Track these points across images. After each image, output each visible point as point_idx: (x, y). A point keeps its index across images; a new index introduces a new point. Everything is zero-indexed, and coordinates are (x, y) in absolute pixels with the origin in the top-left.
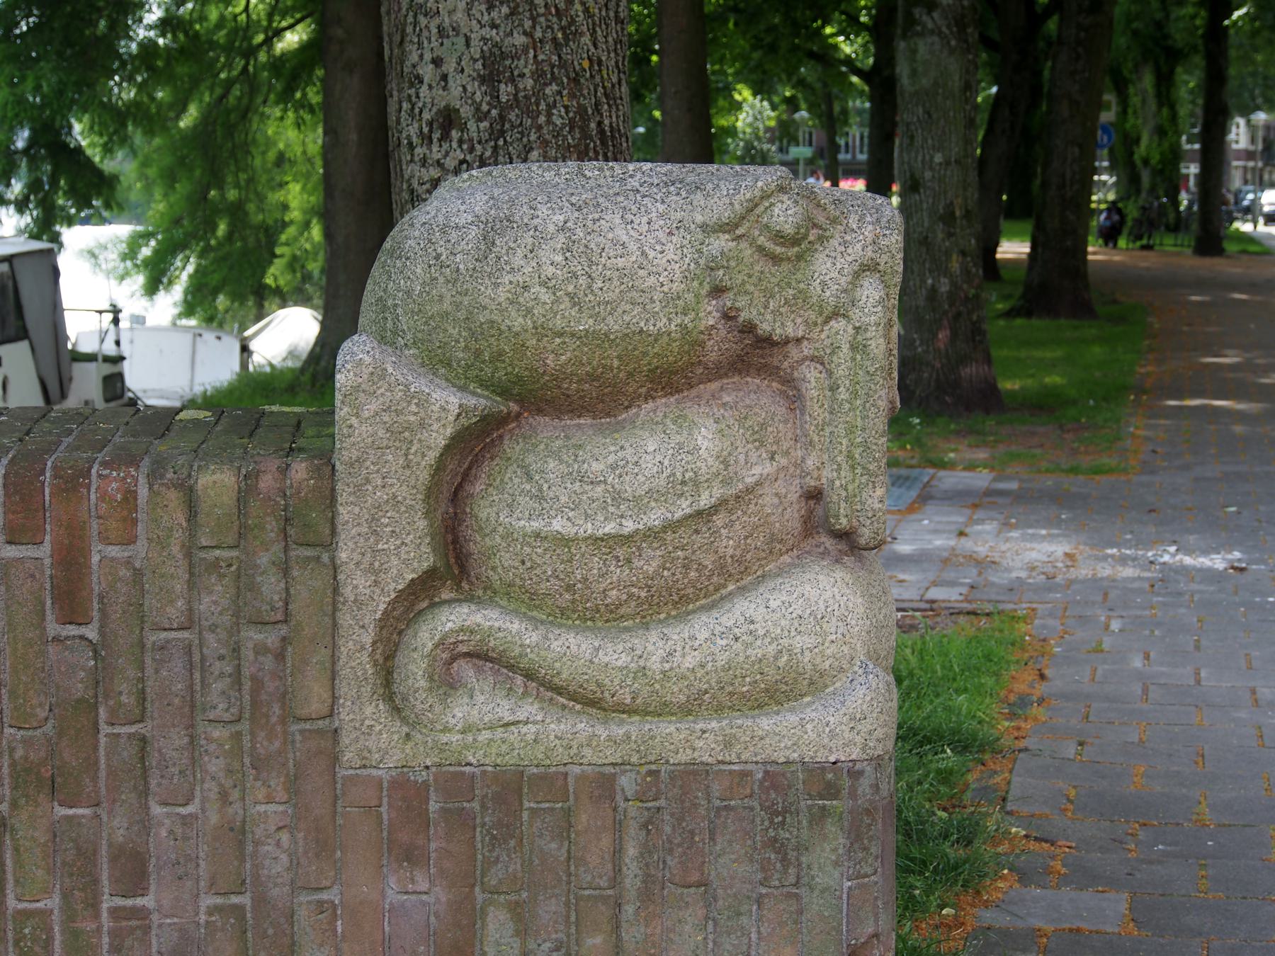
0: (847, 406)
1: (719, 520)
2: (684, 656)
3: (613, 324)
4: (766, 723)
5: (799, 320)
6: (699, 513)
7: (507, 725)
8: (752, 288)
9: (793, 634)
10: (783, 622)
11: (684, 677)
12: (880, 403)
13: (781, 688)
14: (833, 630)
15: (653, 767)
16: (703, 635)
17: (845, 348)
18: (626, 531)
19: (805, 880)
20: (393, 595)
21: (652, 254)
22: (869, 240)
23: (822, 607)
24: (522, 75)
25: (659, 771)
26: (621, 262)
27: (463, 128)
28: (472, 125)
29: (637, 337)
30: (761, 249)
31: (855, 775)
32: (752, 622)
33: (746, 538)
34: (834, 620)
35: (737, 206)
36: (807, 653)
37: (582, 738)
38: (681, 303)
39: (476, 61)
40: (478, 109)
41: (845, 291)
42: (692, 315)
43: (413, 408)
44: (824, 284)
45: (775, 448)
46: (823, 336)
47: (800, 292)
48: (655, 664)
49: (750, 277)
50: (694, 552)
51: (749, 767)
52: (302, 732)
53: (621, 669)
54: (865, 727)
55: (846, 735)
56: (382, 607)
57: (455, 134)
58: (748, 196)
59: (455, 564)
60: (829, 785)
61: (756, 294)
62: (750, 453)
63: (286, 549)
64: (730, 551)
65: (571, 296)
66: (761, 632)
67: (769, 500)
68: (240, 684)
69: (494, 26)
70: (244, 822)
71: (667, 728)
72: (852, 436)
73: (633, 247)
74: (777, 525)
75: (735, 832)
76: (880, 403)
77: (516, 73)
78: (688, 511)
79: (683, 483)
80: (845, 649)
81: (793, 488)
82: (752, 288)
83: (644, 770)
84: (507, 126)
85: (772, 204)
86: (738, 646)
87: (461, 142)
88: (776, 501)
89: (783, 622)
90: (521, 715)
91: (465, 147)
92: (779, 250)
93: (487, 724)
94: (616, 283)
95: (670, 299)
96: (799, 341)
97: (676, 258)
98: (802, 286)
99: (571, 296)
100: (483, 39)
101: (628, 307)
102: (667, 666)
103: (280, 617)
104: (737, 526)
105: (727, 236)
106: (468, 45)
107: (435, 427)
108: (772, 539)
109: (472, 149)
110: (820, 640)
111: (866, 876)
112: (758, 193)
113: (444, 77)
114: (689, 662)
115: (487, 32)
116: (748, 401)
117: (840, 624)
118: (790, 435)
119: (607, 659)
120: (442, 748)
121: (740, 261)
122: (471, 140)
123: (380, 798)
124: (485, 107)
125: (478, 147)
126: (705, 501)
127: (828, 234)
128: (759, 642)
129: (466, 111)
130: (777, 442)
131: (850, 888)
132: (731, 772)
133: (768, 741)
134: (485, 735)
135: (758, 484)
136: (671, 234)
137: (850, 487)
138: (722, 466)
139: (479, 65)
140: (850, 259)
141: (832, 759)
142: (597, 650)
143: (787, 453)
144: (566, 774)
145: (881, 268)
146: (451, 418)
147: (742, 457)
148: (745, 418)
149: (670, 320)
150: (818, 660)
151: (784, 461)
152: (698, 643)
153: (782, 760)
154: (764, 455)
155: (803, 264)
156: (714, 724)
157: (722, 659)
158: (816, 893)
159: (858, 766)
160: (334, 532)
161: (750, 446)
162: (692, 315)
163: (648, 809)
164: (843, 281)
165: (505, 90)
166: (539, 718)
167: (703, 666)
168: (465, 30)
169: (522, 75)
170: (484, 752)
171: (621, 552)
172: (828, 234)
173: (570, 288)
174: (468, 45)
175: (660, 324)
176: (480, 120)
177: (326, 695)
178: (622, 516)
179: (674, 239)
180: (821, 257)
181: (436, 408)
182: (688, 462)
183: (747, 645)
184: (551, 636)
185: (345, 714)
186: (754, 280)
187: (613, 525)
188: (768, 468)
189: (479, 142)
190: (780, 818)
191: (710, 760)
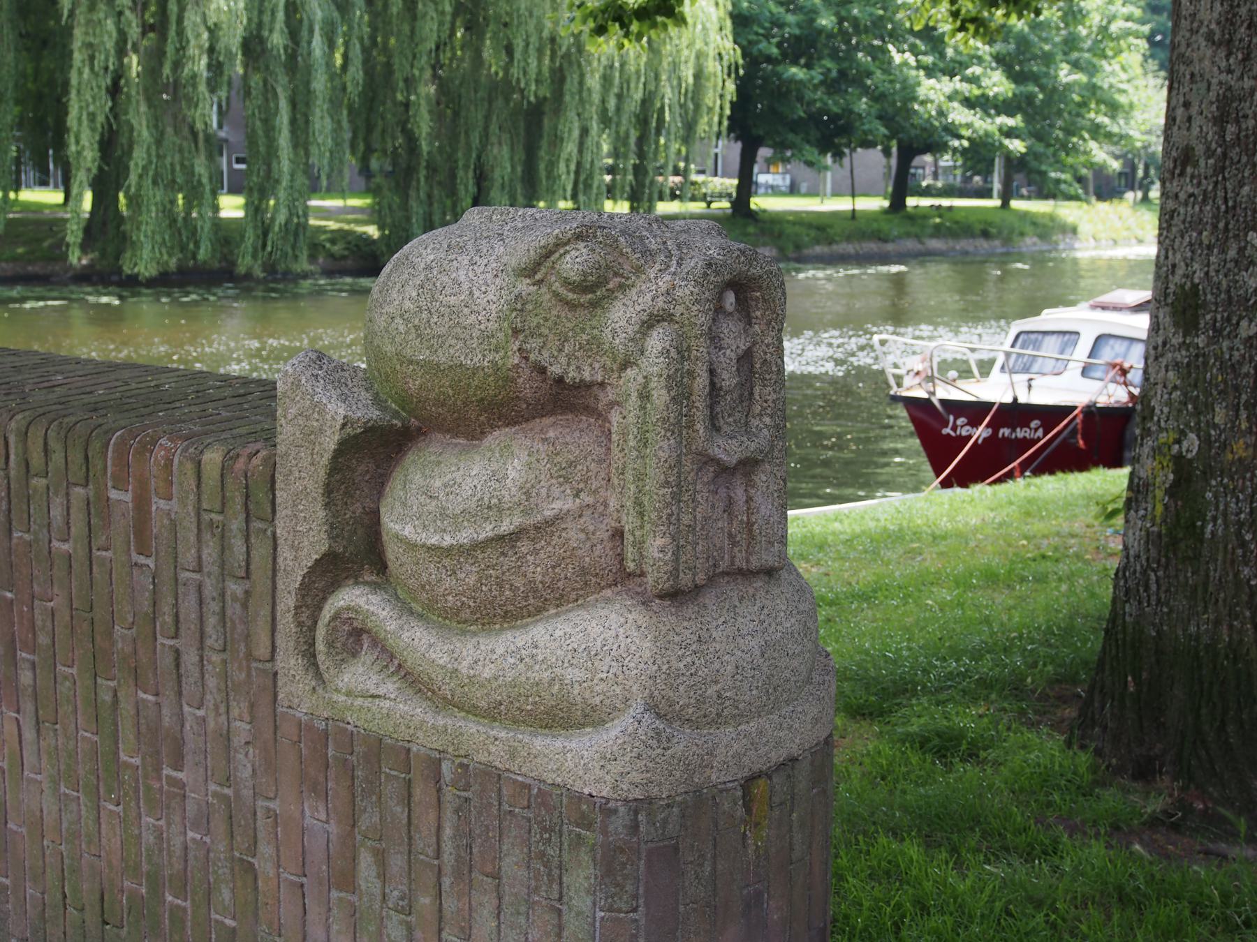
0: (635, 453)
1: (524, 546)
2: (484, 666)
3: (442, 357)
4: (540, 743)
5: (597, 365)
6: (500, 538)
7: (373, 696)
8: (546, 332)
9: (566, 665)
10: (559, 652)
11: (483, 686)
12: (661, 453)
13: (560, 716)
14: (605, 668)
15: (465, 761)
16: (500, 651)
17: (634, 395)
18: (445, 544)
19: (565, 899)
20: (306, 570)
21: (477, 293)
22: (663, 290)
23: (599, 644)
24: (1246, 117)
25: (468, 766)
26: (452, 300)
27: (1196, 165)
28: (1202, 163)
29: (459, 370)
30: (556, 294)
31: (608, 812)
32: (536, 647)
33: (554, 567)
34: (608, 659)
35: (532, 252)
36: (576, 686)
37: (417, 720)
38: (493, 341)
39: (1212, 103)
40: (1208, 148)
41: (633, 340)
42: (502, 354)
43: (316, 415)
44: (614, 331)
45: (582, 485)
46: (621, 383)
47: (593, 338)
48: (464, 667)
49: (546, 320)
50: (503, 573)
51: (528, 781)
52: (257, 668)
53: (443, 667)
54: (616, 768)
55: (597, 771)
56: (300, 578)
57: (1189, 170)
58: (542, 243)
59: (359, 552)
60: (583, 816)
61: (551, 337)
62: (553, 488)
63: (247, 520)
64: (540, 578)
65: (417, 328)
66: (540, 658)
67: (573, 534)
68: (225, 623)
69: (1230, 71)
70: (228, 731)
71: (472, 728)
72: (640, 484)
73: (465, 286)
74: (587, 559)
75: (516, 837)
76: (661, 453)
77: (1241, 114)
78: (490, 534)
79: (489, 508)
80: (618, 690)
81: (603, 526)
82: (546, 332)
83: (458, 761)
84: (1227, 163)
85: (567, 252)
86: (521, 666)
87: (1192, 177)
88: (582, 536)
89: (559, 652)
90: (381, 691)
91: (1195, 181)
92: (571, 296)
93: (362, 693)
94: (447, 319)
95: (486, 336)
96: (602, 385)
97: (495, 299)
98: (596, 332)
99: (417, 328)
100: (1220, 83)
101: (453, 342)
102: (472, 672)
103: (243, 574)
104: (542, 555)
105: (528, 281)
106: (1209, 89)
107: (328, 433)
108: (583, 571)
109: (1199, 184)
110: (589, 676)
111: (620, 911)
112: (552, 240)
113: (1189, 119)
114: (487, 673)
115: (1223, 77)
116: (568, 439)
117: (614, 664)
118: (602, 474)
119: (434, 656)
120: (332, 704)
121: (538, 304)
122: (1199, 175)
123: (300, 736)
124: (1214, 146)
125: (1204, 181)
126: (506, 527)
127: (629, 282)
128: (537, 667)
129: (1200, 149)
130: (586, 481)
131: (602, 918)
132: (515, 781)
133: (539, 760)
134: (359, 701)
135: (558, 518)
136: (496, 276)
137: (637, 533)
138: (524, 497)
139: (1214, 108)
140: (638, 308)
141: (586, 791)
142: (431, 646)
143: (595, 492)
144: (409, 750)
145: (677, 319)
146: (338, 427)
147: (544, 492)
148: (557, 454)
149: (484, 356)
150: (587, 695)
151: (589, 500)
152: (494, 657)
153: (550, 781)
154: (568, 491)
155: (599, 311)
156: (503, 734)
157: (510, 675)
158: (573, 914)
159: (611, 805)
160: (274, 512)
161: (554, 481)
162: (502, 354)
163: (459, 797)
164: (630, 329)
165: (1231, 129)
166: (393, 696)
167: (496, 679)
168: (1207, 76)
169: (1246, 117)
170: (361, 716)
171: (446, 562)
172: (629, 282)
173: (416, 322)
174: (1209, 89)
175: (475, 360)
176: (1209, 158)
177: (268, 643)
178: (445, 531)
179: (498, 281)
180: (618, 304)
181: (328, 417)
182: (495, 489)
183: (529, 668)
184: (406, 627)
185: (280, 664)
186: (549, 324)
187: (437, 537)
188: (569, 504)
189: (1206, 178)
190: (547, 835)
191: (500, 766)
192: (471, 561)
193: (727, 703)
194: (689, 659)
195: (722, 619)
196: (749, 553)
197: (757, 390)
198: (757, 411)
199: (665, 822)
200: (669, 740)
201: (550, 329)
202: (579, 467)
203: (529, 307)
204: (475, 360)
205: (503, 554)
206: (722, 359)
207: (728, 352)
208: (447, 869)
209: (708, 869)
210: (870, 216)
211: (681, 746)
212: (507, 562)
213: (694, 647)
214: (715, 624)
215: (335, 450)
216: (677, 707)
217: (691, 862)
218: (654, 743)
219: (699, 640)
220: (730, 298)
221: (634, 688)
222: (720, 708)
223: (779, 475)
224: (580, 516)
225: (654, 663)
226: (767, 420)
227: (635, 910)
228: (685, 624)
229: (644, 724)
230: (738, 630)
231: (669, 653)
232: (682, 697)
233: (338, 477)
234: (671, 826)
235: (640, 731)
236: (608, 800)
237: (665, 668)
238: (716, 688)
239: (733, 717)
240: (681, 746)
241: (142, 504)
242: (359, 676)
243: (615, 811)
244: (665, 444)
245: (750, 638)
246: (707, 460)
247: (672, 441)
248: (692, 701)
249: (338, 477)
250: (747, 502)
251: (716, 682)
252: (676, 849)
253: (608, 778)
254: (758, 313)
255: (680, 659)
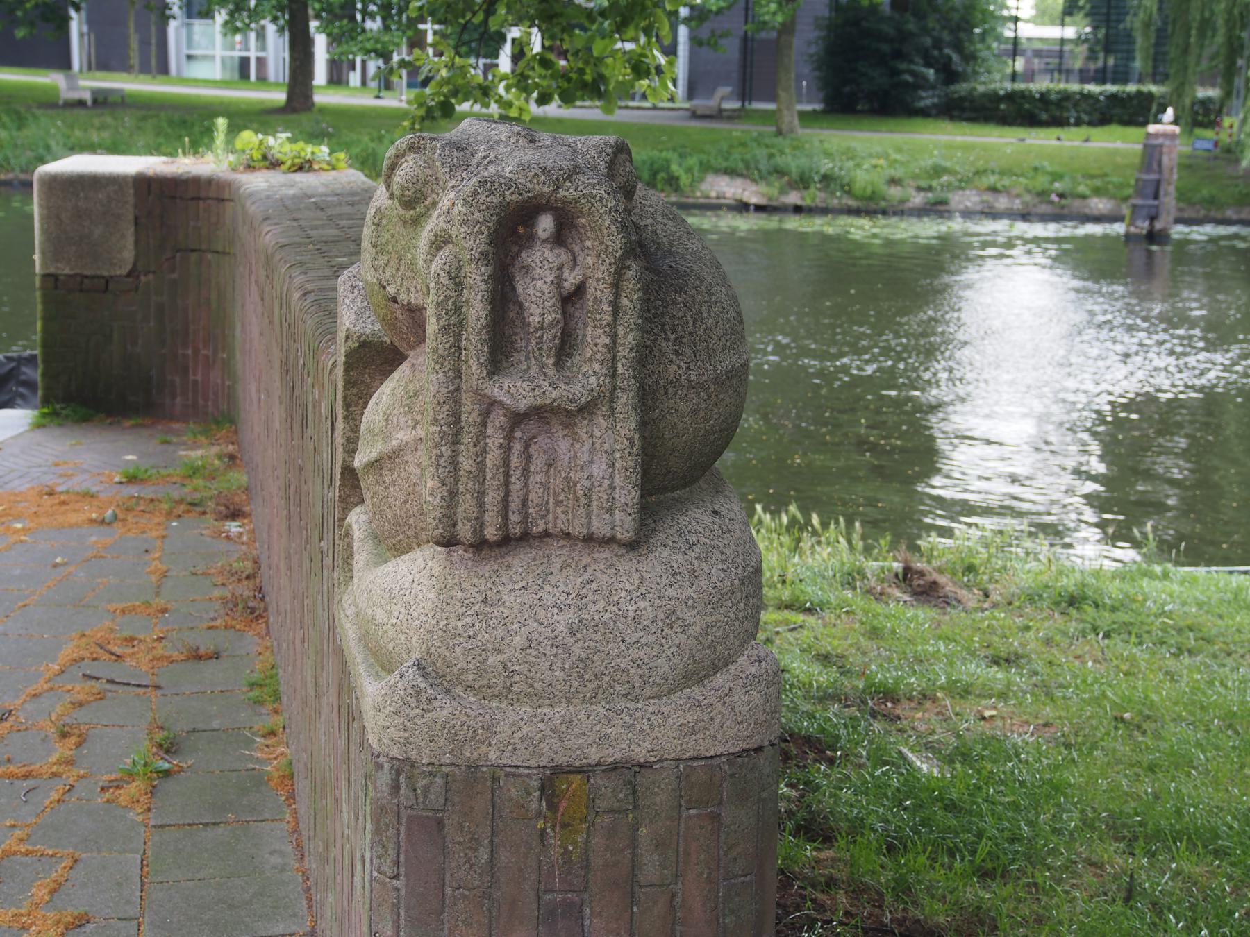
45: (419, 417)
193: (517, 678)
194: (469, 620)
195: (524, 584)
199: (426, 790)
200: (429, 702)
203: (384, 222)
206: (531, 291)
207: (539, 283)
209: (484, 856)
211: (445, 712)
213: (476, 607)
214: (510, 587)
216: (455, 670)
217: (459, 843)
218: (413, 701)
219: (485, 601)
221: (414, 640)
222: (508, 682)
223: (623, 432)
224: (416, 450)
225: (434, 617)
226: (597, 366)
227: (396, 877)
228: (475, 581)
229: (406, 679)
231: (449, 608)
232: (459, 659)
233: (355, 391)
234: (433, 797)
235: (400, 685)
237: (442, 623)
238: (500, 657)
240: (445, 712)
244: (433, 377)
245: (555, 610)
247: (441, 375)
248: (470, 666)
249: (355, 391)
251: (500, 651)
252: (440, 823)
255: (460, 617)
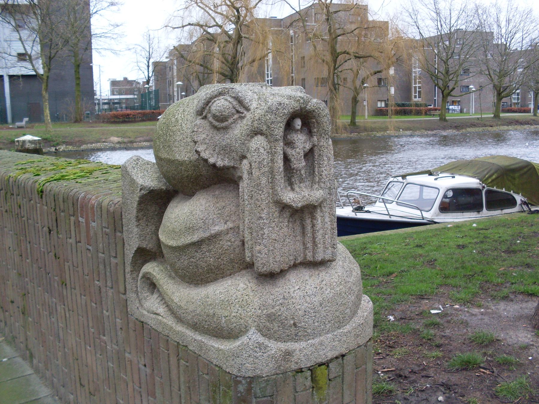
1: (204, 248)
85: (215, 101)
103: (114, 255)
105: (200, 117)
143: (234, 221)
144: (168, 340)
154: (222, 221)
192: (184, 254)
193: (300, 329)
196: (314, 254)
197: (316, 169)
198: (317, 181)
201: (209, 140)
202: (227, 209)
204: (182, 157)
205: (196, 251)
208: (183, 396)
210: (487, 119)
212: (198, 255)
214: (293, 290)
215: (139, 201)
219: (284, 298)
220: (298, 123)
224: (228, 233)
230: (307, 293)
236: (237, 376)
239: (304, 336)
241: (87, 223)
242: (152, 303)
243: (240, 382)
246: (284, 207)
249: (142, 213)
250: (312, 227)
253: (235, 366)
254: (315, 130)
